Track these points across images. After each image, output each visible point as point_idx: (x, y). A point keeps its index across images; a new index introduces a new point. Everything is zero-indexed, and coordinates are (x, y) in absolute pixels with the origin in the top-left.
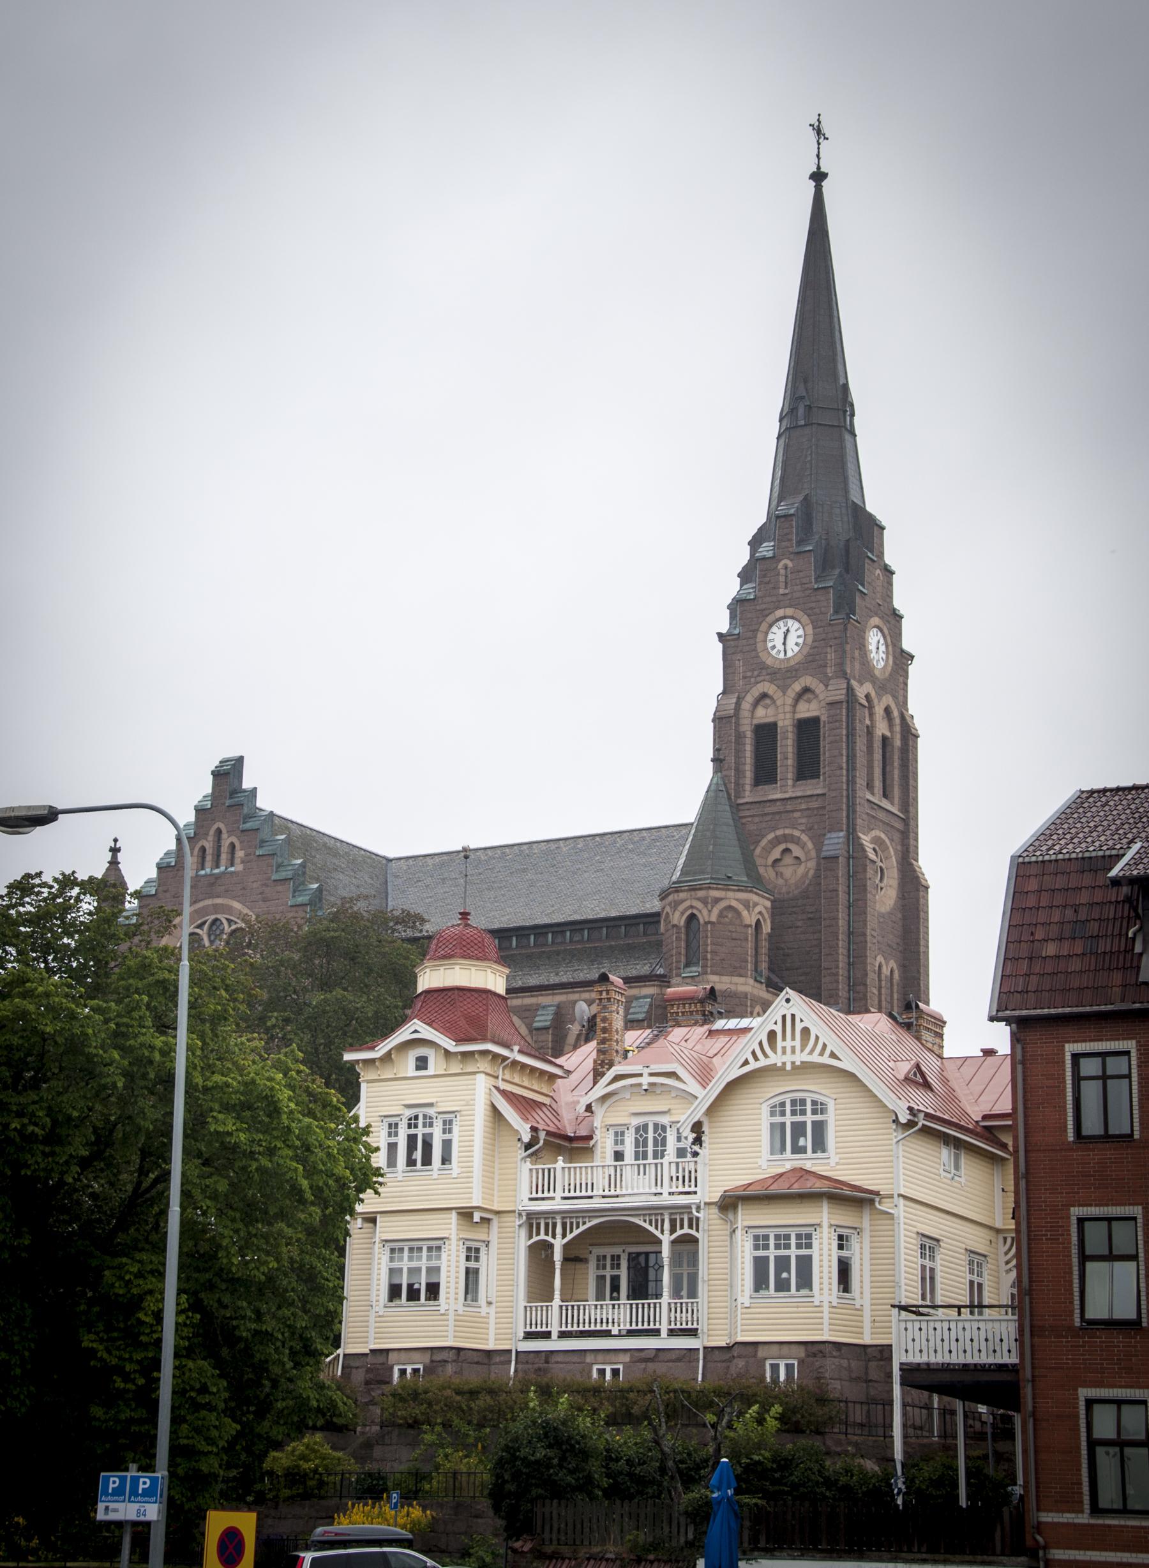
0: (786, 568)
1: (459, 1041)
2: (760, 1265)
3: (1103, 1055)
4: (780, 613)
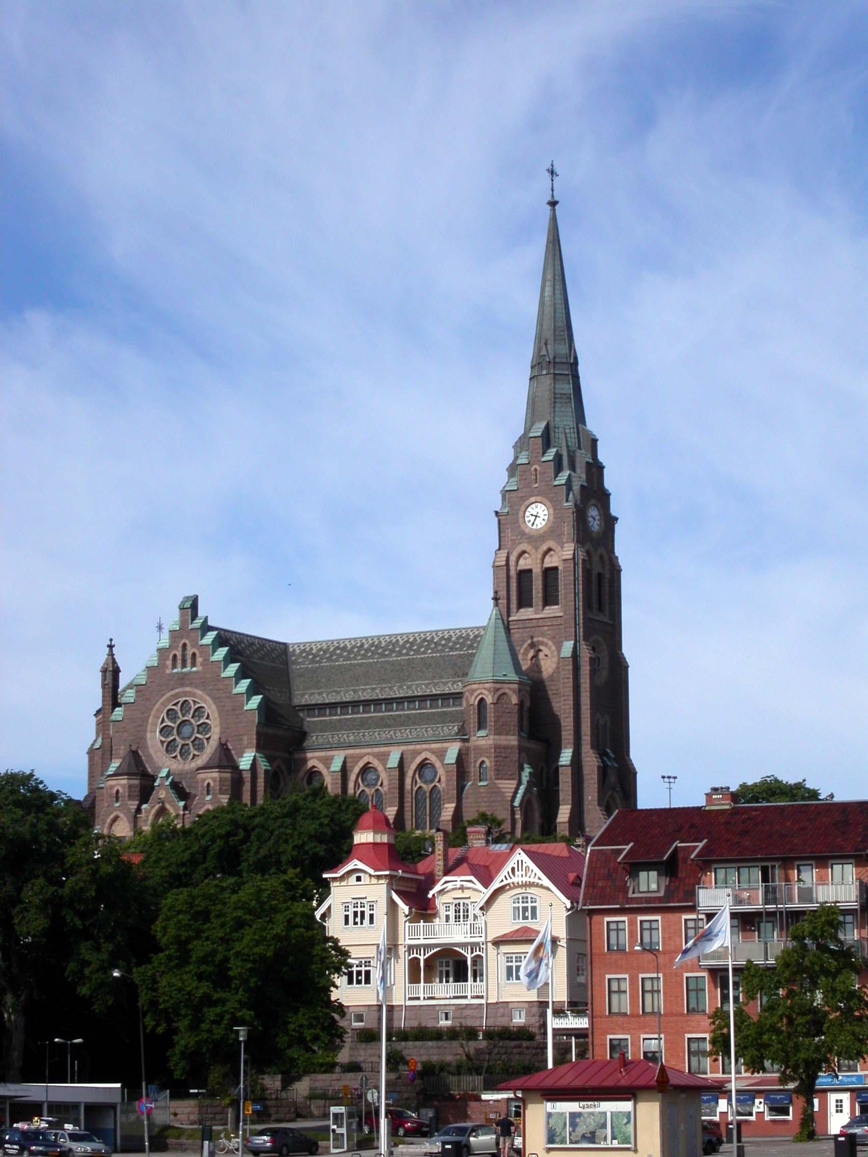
0: (536, 470)
1: (376, 870)
2: (509, 969)
3: (617, 922)
4: (533, 499)
